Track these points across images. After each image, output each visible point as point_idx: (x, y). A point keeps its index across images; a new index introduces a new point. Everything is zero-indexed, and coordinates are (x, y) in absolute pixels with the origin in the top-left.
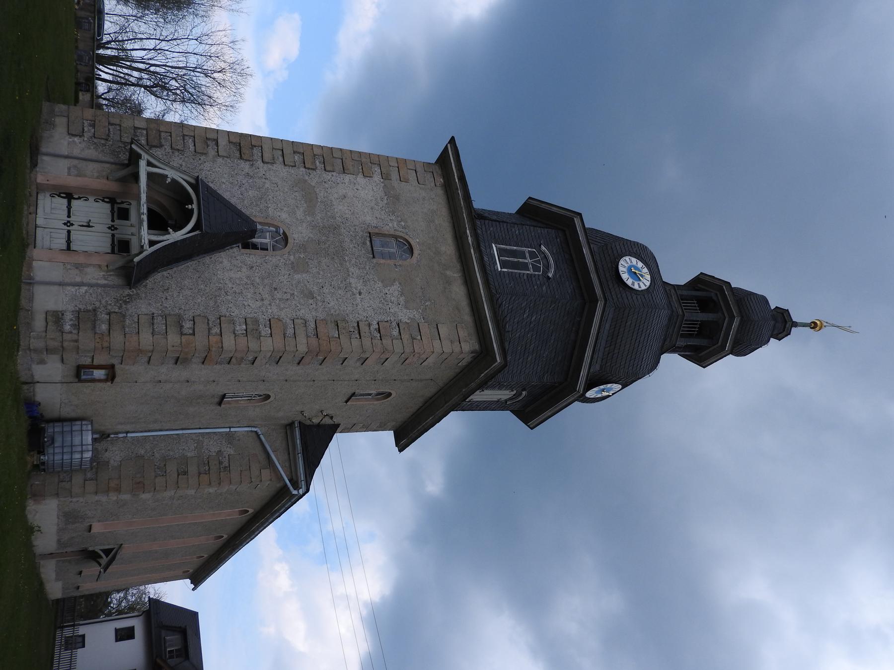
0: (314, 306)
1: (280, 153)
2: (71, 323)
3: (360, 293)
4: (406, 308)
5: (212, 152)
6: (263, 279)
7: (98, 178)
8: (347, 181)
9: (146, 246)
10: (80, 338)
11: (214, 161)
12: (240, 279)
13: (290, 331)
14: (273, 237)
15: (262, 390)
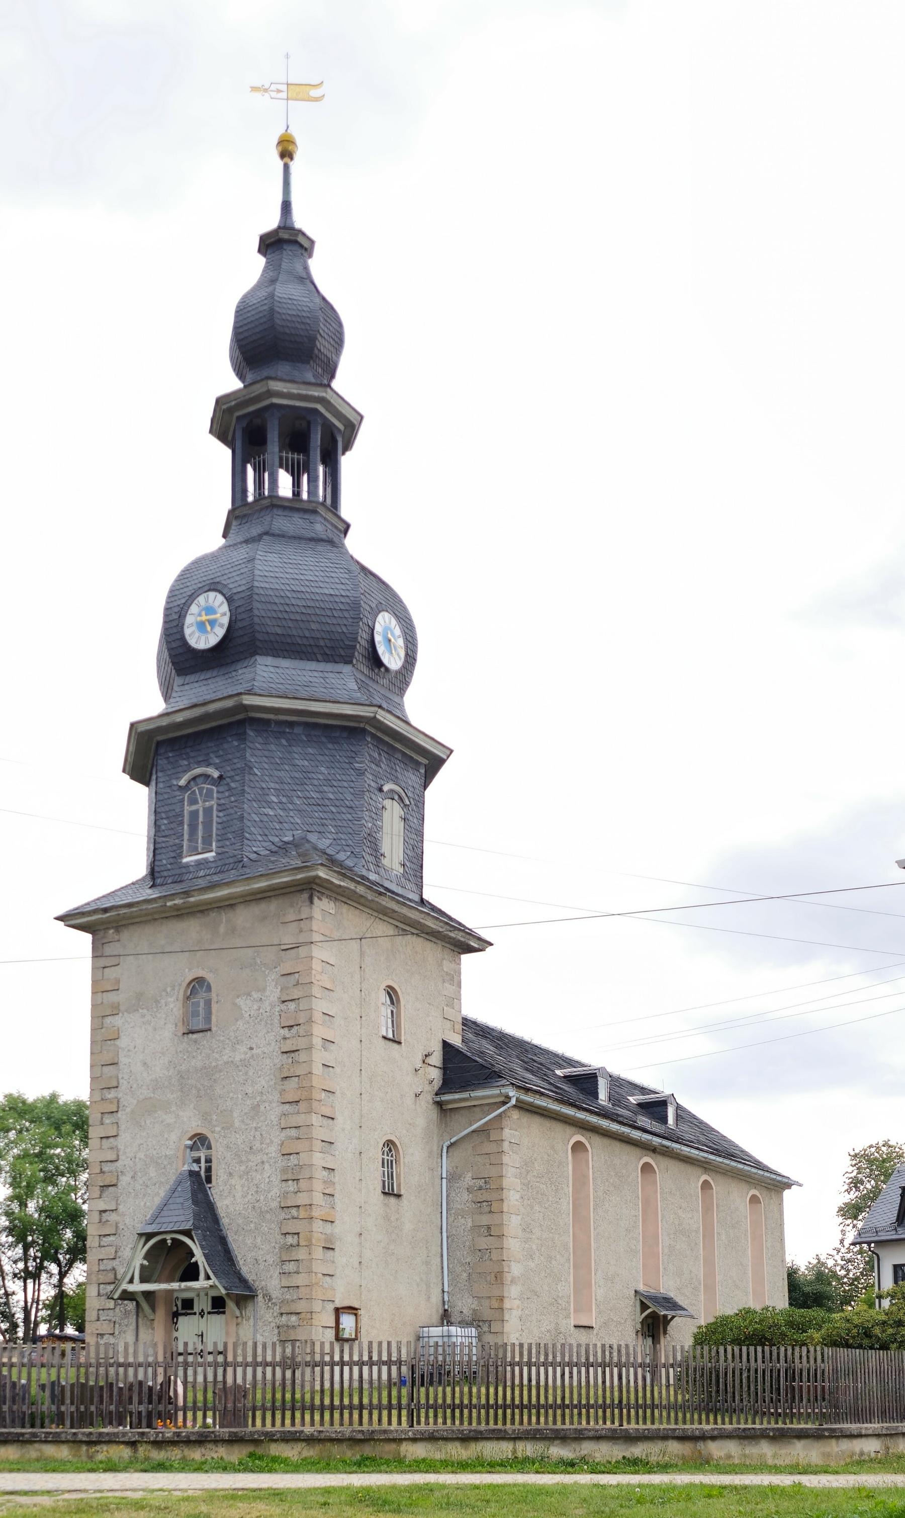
0: (267, 1105)
1: (104, 1140)
3: (251, 1049)
4: (264, 990)
5: (113, 1217)
7: (153, 1329)
9: (210, 1282)
11: (123, 1215)
12: (243, 1186)
13: (293, 1133)
14: (198, 1149)
15: (376, 1154)
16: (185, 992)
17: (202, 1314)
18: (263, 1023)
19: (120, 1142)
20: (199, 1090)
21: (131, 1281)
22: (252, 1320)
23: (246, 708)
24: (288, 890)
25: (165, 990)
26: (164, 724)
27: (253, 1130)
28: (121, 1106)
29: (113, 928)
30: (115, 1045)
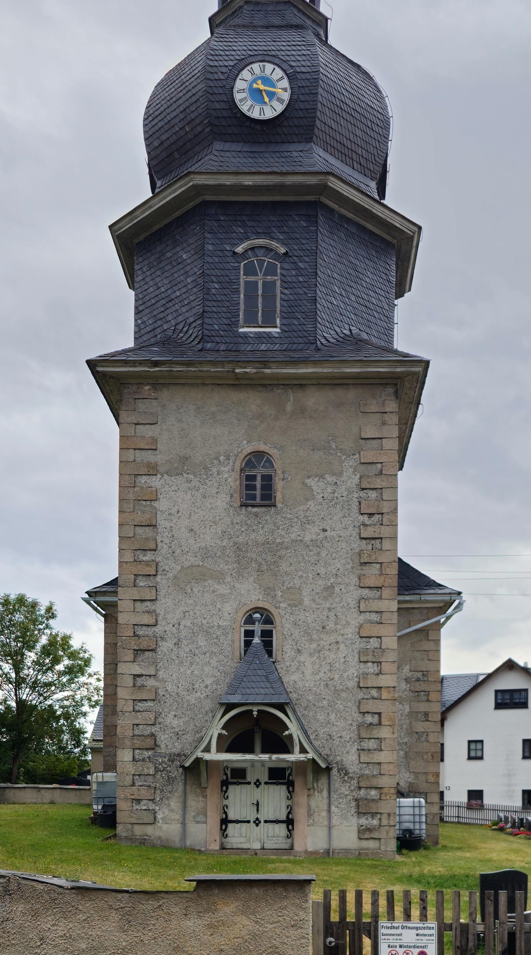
0: (342, 587)
1: (138, 604)
2: (370, 819)
4: (341, 474)
5: (151, 683)
6: (312, 640)
7: (205, 797)
8: (168, 524)
10: (386, 811)
11: (164, 681)
12: (313, 664)
13: (374, 617)
16: (241, 464)
17: (258, 784)
18: (338, 507)
19: (160, 607)
20: (260, 564)
21: (207, 750)
22: (325, 793)
23: (324, 189)
24: (374, 381)
25: (217, 458)
26: (228, 183)
27: (327, 610)
28: (160, 570)
29: (148, 384)
30: (151, 506)
